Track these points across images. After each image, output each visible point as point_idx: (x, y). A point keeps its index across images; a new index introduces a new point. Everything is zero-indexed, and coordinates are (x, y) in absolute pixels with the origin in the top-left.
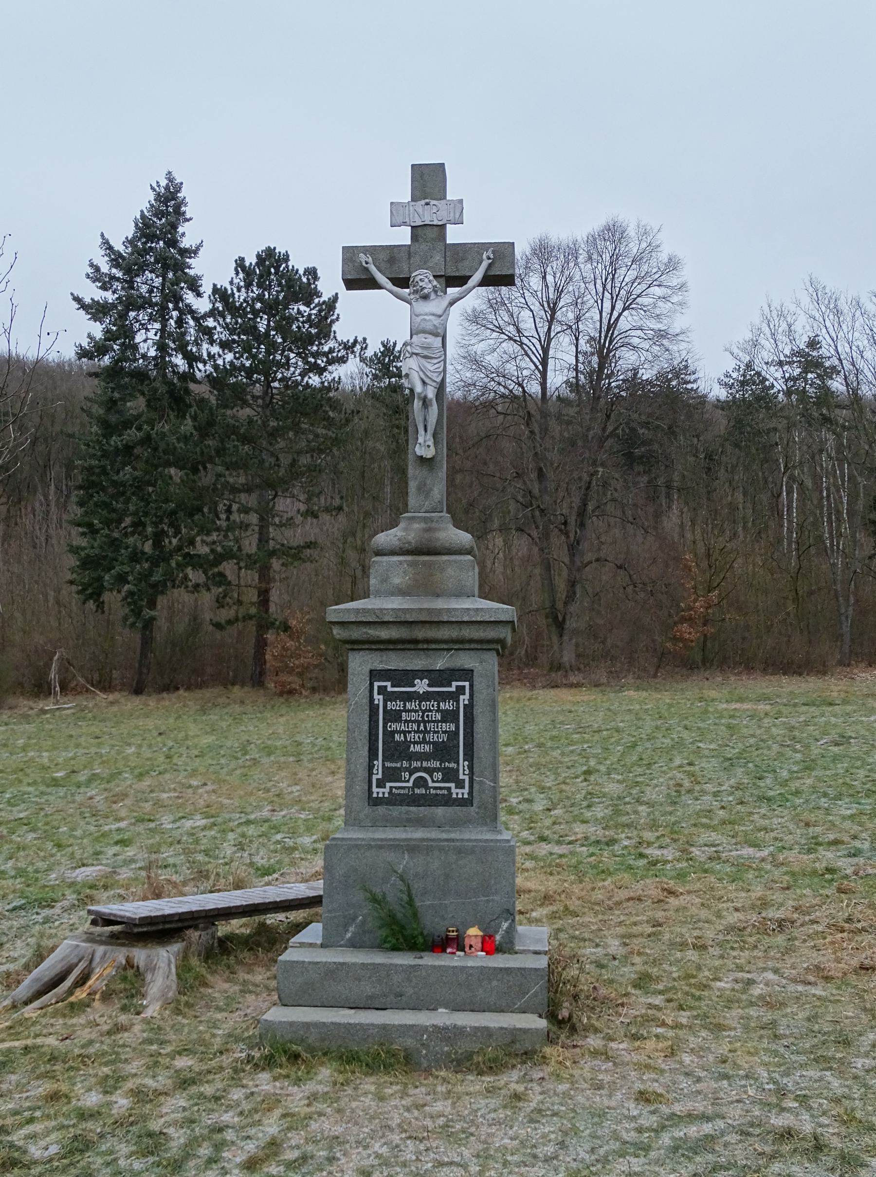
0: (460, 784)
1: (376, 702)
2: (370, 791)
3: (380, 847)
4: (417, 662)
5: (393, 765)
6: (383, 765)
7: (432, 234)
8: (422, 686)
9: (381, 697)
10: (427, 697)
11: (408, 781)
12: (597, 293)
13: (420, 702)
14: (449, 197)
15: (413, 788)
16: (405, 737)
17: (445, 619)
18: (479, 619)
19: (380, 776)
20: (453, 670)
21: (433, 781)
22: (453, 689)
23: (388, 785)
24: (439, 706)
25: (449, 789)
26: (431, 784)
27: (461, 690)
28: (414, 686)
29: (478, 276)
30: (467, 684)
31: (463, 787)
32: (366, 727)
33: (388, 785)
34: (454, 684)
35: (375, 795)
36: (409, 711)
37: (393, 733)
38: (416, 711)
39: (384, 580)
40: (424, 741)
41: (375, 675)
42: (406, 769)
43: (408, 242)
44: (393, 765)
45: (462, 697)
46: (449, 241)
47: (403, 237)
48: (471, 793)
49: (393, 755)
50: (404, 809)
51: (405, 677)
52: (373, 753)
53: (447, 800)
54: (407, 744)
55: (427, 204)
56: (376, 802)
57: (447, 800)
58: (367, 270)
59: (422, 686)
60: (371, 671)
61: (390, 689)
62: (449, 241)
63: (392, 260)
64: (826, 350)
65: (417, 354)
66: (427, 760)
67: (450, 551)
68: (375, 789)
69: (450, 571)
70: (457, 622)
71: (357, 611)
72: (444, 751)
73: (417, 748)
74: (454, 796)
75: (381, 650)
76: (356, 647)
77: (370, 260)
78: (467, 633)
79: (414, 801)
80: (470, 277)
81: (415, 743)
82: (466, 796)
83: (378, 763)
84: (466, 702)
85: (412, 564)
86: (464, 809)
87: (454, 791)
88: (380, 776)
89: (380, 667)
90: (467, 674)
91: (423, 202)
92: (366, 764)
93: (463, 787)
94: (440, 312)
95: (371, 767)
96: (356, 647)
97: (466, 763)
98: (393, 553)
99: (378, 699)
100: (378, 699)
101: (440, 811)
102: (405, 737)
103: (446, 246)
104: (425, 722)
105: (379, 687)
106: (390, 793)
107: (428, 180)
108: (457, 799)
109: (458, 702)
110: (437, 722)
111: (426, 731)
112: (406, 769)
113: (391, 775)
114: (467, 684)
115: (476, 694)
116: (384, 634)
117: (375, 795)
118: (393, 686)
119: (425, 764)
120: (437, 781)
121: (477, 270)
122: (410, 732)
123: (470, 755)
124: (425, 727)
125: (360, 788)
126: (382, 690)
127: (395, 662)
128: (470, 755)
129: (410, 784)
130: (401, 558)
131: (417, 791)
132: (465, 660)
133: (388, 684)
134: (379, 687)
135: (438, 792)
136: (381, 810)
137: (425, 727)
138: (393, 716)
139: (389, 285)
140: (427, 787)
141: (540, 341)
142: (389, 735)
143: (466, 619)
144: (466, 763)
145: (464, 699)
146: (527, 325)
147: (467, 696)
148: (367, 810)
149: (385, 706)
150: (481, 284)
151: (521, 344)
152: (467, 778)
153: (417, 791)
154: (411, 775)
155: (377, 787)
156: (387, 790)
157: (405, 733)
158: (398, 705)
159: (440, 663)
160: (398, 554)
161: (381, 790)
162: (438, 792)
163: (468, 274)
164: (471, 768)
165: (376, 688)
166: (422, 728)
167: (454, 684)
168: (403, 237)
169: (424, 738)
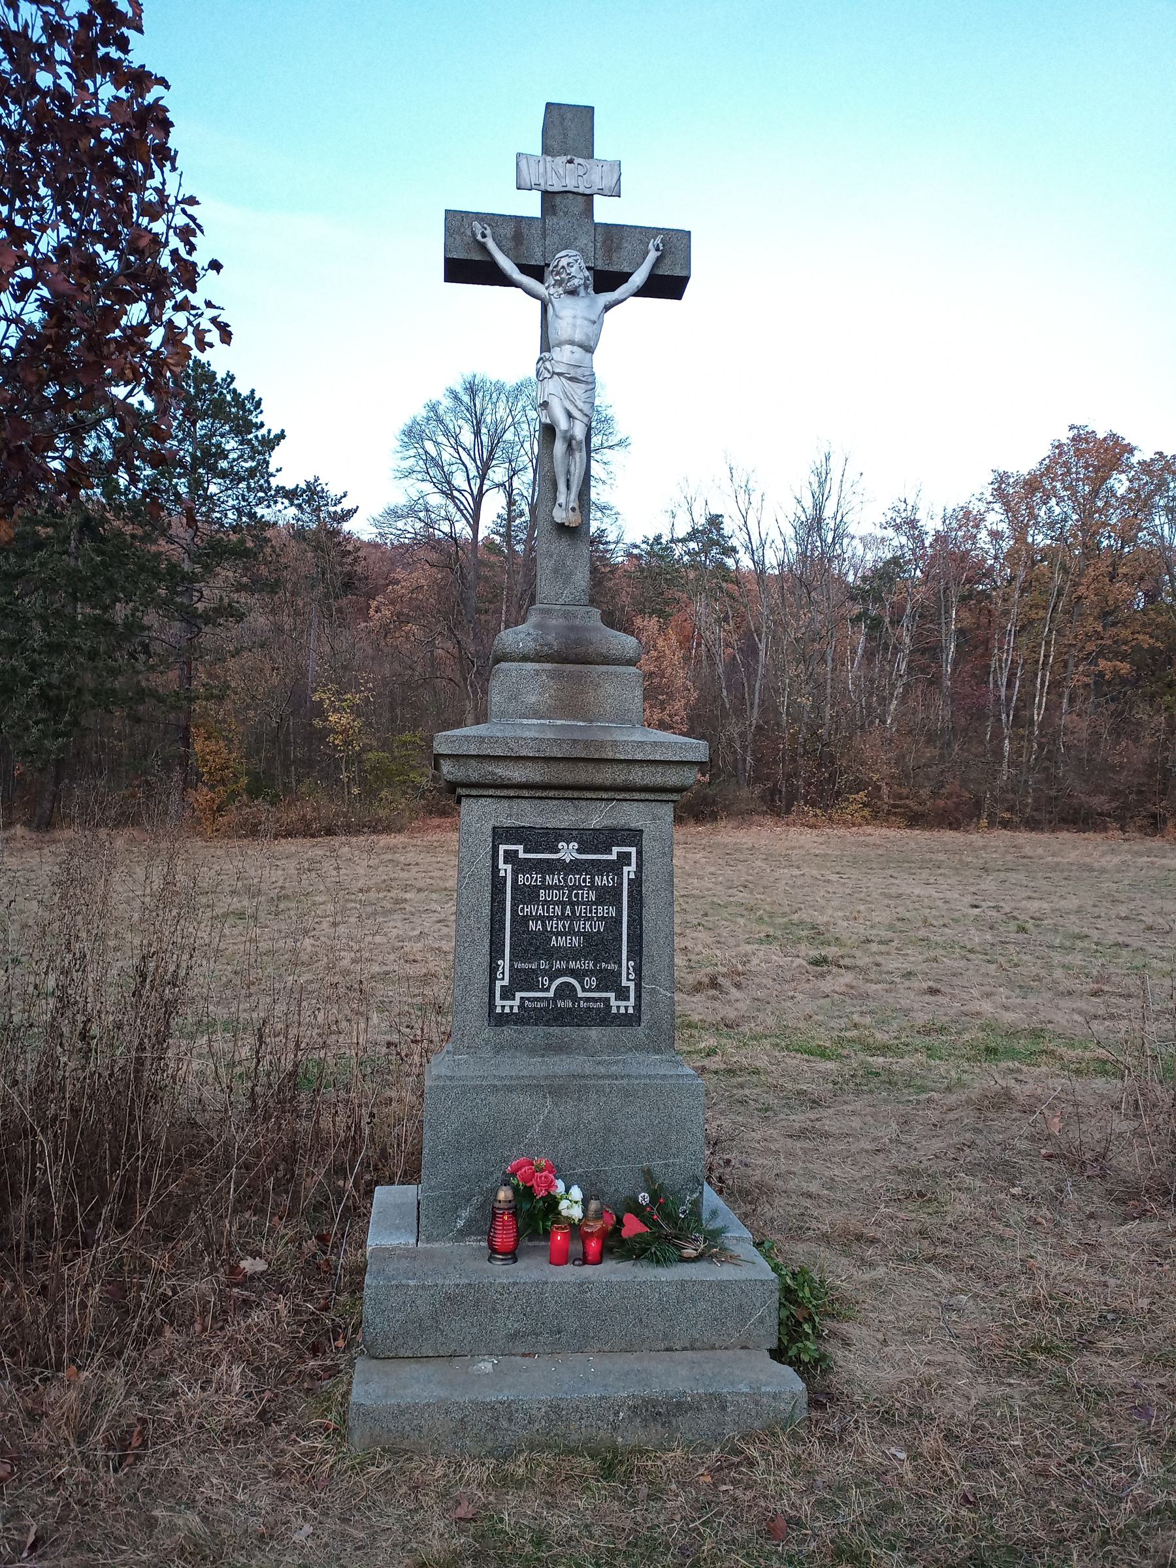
0: (622, 994)
1: (502, 874)
2: (491, 1005)
3: (510, 1089)
4: (560, 816)
5: (526, 966)
6: (511, 966)
7: (577, 206)
8: (568, 852)
9: (509, 867)
10: (575, 867)
11: (548, 990)
12: (532, 453)
13: (566, 875)
14: (598, 154)
15: (554, 999)
16: (544, 925)
17: (610, 755)
18: (658, 758)
19: (506, 982)
20: (613, 830)
21: (584, 990)
22: (614, 857)
23: (518, 995)
24: (592, 882)
25: (608, 999)
26: (580, 994)
27: (624, 858)
28: (558, 851)
29: (639, 278)
30: (633, 850)
31: (627, 999)
32: (487, 911)
33: (518, 995)
34: (615, 849)
35: (499, 1010)
36: (550, 887)
37: (526, 919)
38: (559, 888)
39: (514, 697)
40: (571, 932)
41: (500, 835)
42: (545, 972)
43: (537, 213)
44: (526, 966)
45: (626, 869)
46: (598, 218)
47: (530, 205)
48: (638, 1007)
49: (526, 951)
50: (541, 1030)
51: (547, 838)
52: (496, 951)
53: (604, 1017)
54: (545, 935)
55: (571, 162)
56: (500, 1020)
57: (604, 1017)
58: (483, 247)
59: (568, 852)
60: (494, 828)
61: (521, 855)
62: (598, 218)
63: (518, 238)
64: (728, 527)
65: (559, 374)
66: (575, 959)
67: (607, 660)
68: (498, 1002)
69: (609, 688)
70: (625, 760)
71: (482, 740)
72: (601, 946)
73: (561, 941)
74: (614, 1010)
75: (509, 797)
76: (474, 792)
77: (488, 232)
78: (638, 776)
79: (555, 1019)
80: (631, 274)
81: (558, 934)
82: (631, 1011)
83: (505, 964)
84: (632, 876)
85: (552, 675)
86: (629, 1030)
87: (613, 1003)
88: (506, 982)
89: (508, 823)
90: (634, 836)
91: (564, 159)
92: (486, 965)
93: (627, 999)
94: (594, 318)
95: (493, 970)
96: (474, 792)
97: (631, 963)
98: (525, 658)
99: (506, 869)
100: (506, 869)
101: (594, 1033)
102: (544, 925)
103: (597, 225)
104: (572, 904)
105: (506, 851)
106: (521, 1006)
107: (568, 129)
108: (618, 1016)
109: (620, 875)
110: (590, 903)
111: (573, 917)
112: (545, 972)
113: (523, 980)
114: (633, 850)
115: (647, 866)
116: (517, 774)
117: (499, 1010)
118: (629, 865)
119: (572, 965)
120: (590, 990)
121: (639, 265)
122: (550, 918)
123: (636, 951)
124: (573, 912)
125: (476, 1001)
126: (510, 857)
127: (529, 814)
128: (636, 951)
129: (551, 994)
130: (536, 666)
131: (560, 1004)
132: (631, 814)
133: (520, 848)
134: (506, 851)
135: (592, 1005)
136: (508, 1032)
137: (573, 912)
138: (525, 895)
139: (516, 275)
140: (575, 999)
141: (472, 494)
142: (520, 922)
143: (639, 757)
144: (631, 963)
145: (629, 871)
146: (459, 480)
147: (633, 868)
148: (487, 1033)
149: (515, 881)
150: (642, 292)
151: (453, 498)
152: (632, 985)
153: (560, 1004)
154: (551, 981)
155: (502, 998)
156: (517, 1002)
157: (542, 919)
158: (535, 879)
159: (597, 817)
160: (532, 661)
161: (508, 1003)
162: (592, 1005)
163: (627, 270)
164: (638, 970)
165: (501, 853)
166: (568, 912)
167: (615, 849)
168: (530, 205)
169: (571, 927)
